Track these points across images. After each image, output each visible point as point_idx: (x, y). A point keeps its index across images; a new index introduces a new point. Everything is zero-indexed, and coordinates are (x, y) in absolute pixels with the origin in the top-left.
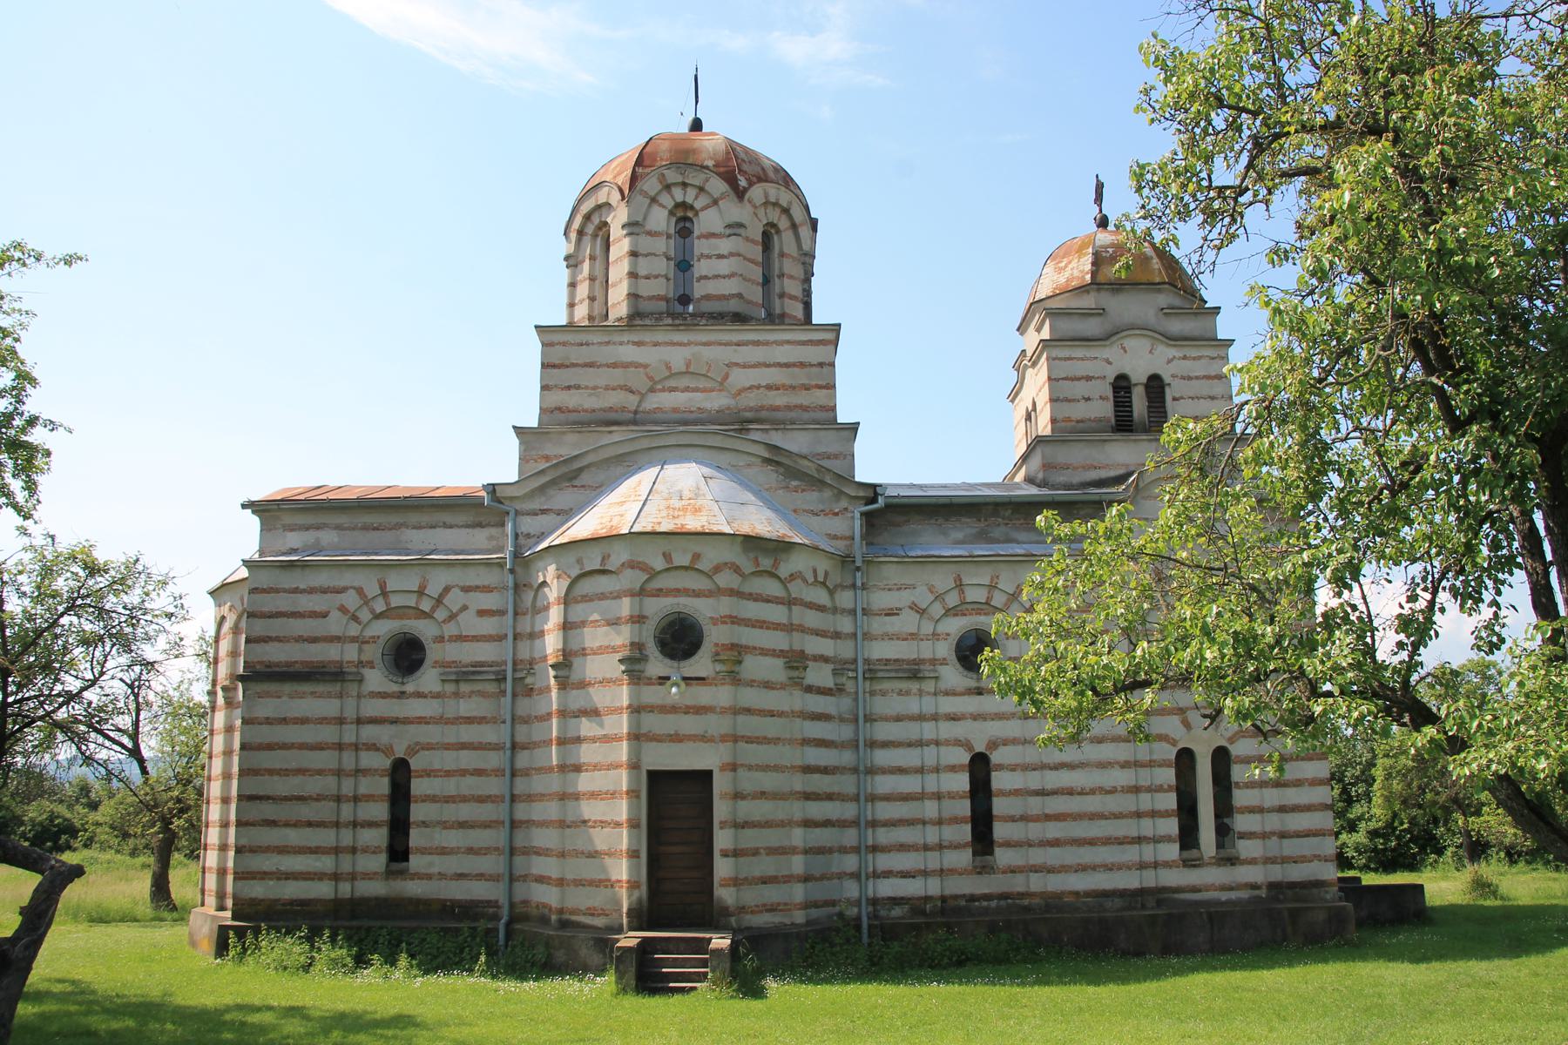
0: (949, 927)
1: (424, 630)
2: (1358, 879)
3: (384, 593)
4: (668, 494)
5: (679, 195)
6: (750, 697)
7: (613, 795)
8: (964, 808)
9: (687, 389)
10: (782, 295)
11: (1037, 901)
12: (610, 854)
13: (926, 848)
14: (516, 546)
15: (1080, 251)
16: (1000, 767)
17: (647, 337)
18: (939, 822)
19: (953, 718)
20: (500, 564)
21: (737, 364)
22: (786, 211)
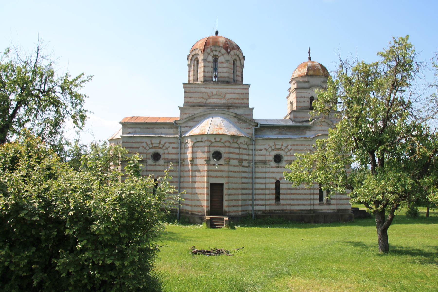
0: (270, 216)
1: (160, 151)
2: (358, 208)
3: (152, 143)
4: (213, 125)
5: (214, 53)
6: (232, 168)
7: (203, 188)
8: (274, 192)
9: (216, 98)
10: (237, 76)
11: (288, 211)
12: (202, 200)
13: (266, 200)
14: (181, 134)
15: (304, 66)
16: (282, 183)
17: (208, 86)
18: (269, 194)
19: (273, 173)
20: (177, 138)
21: (227, 93)
22: (238, 56)
